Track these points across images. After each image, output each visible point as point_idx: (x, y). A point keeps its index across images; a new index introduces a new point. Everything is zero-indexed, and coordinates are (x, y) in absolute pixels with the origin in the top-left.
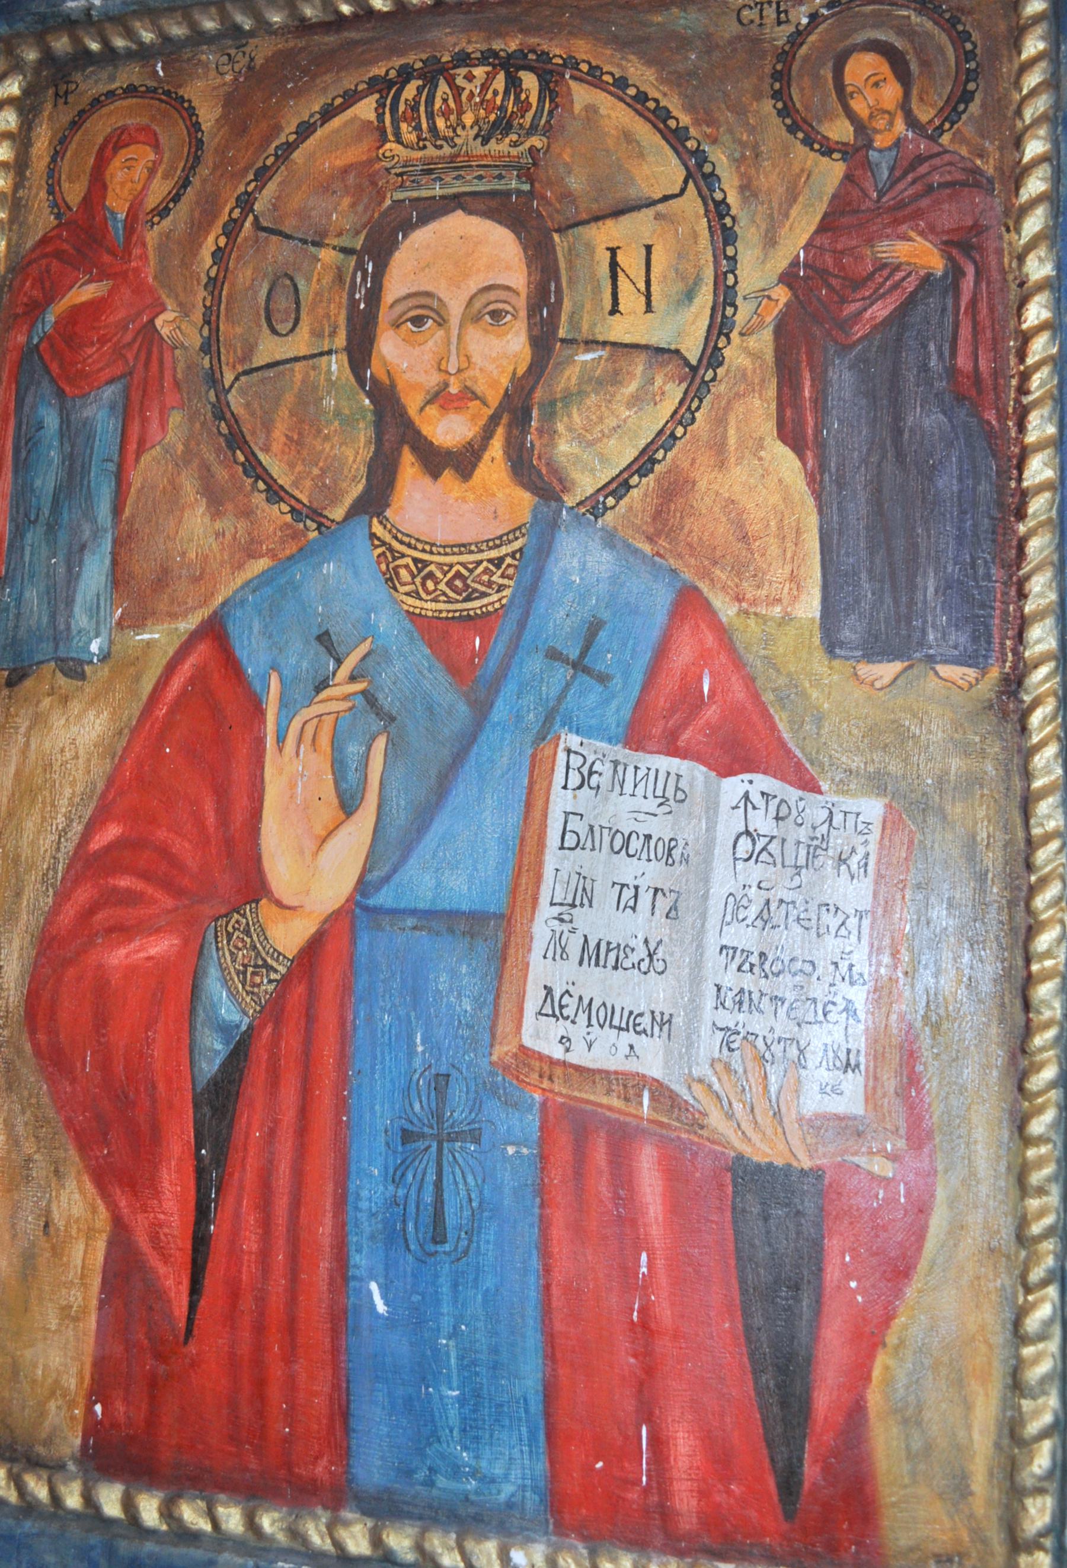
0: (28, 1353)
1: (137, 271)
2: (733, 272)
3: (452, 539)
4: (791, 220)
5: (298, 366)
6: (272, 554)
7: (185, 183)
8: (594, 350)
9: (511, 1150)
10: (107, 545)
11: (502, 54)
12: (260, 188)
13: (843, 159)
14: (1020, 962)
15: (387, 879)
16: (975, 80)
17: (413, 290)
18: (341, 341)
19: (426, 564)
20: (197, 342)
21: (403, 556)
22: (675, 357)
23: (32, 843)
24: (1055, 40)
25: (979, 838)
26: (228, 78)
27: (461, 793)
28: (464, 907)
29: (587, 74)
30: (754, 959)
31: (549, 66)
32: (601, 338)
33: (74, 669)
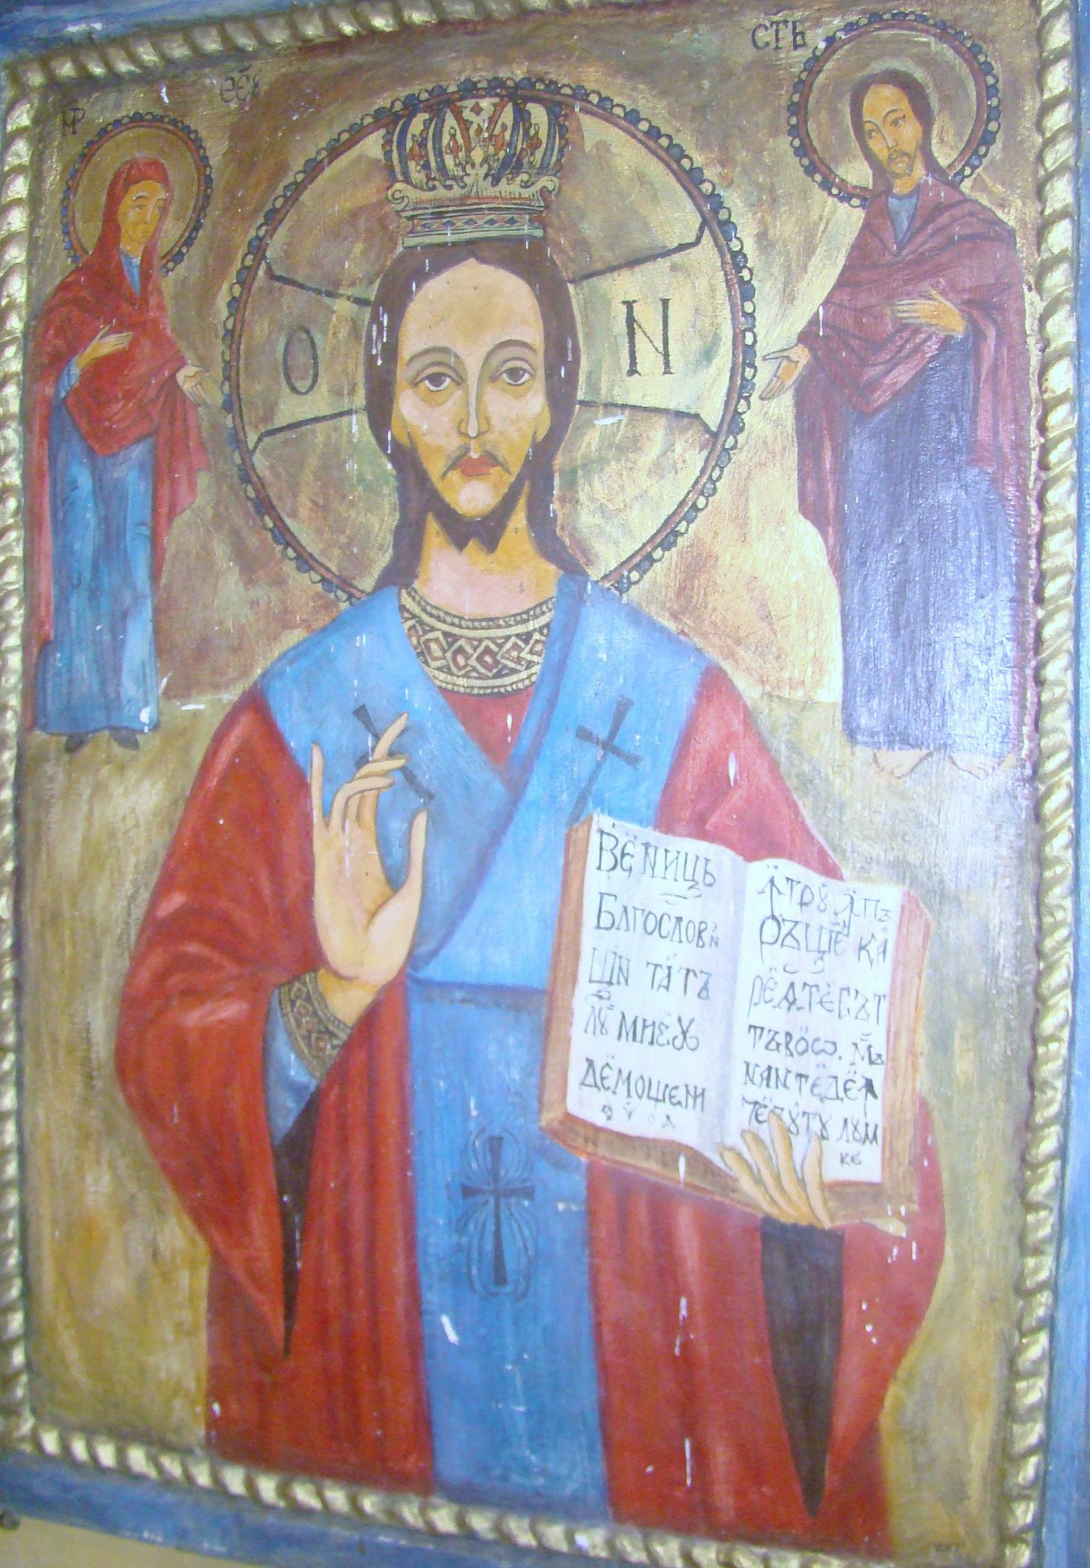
0: (152, 1359)
1: (155, 322)
2: (751, 330)
3: (480, 612)
4: (810, 273)
5: (320, 427)
6: (306, 624)
7: (197, 227)
8: (614, 415)
9: (561, 1206)
10: (147, 613)
11: (510, 83)
12: (271, 234)
13: (862, 206)
14: (1027, 1043)
15: (434, 953)
16: (997, 120)
17: (430, 345)
18: (360, 399)
19: (456, 638)
20: (220, 399)
21: (433, 629)
22: (696, 423)
23: (105, 908)
24: (1078, 77)
25: (991, 926)
26: (233, 105)
27: (502, 869)
28: (509, 981)
29: (597, 106)
30: (781, 1038)
31: (558, 98)
32: (620, 402)
33: (128, 738)
